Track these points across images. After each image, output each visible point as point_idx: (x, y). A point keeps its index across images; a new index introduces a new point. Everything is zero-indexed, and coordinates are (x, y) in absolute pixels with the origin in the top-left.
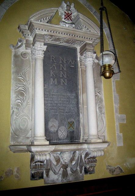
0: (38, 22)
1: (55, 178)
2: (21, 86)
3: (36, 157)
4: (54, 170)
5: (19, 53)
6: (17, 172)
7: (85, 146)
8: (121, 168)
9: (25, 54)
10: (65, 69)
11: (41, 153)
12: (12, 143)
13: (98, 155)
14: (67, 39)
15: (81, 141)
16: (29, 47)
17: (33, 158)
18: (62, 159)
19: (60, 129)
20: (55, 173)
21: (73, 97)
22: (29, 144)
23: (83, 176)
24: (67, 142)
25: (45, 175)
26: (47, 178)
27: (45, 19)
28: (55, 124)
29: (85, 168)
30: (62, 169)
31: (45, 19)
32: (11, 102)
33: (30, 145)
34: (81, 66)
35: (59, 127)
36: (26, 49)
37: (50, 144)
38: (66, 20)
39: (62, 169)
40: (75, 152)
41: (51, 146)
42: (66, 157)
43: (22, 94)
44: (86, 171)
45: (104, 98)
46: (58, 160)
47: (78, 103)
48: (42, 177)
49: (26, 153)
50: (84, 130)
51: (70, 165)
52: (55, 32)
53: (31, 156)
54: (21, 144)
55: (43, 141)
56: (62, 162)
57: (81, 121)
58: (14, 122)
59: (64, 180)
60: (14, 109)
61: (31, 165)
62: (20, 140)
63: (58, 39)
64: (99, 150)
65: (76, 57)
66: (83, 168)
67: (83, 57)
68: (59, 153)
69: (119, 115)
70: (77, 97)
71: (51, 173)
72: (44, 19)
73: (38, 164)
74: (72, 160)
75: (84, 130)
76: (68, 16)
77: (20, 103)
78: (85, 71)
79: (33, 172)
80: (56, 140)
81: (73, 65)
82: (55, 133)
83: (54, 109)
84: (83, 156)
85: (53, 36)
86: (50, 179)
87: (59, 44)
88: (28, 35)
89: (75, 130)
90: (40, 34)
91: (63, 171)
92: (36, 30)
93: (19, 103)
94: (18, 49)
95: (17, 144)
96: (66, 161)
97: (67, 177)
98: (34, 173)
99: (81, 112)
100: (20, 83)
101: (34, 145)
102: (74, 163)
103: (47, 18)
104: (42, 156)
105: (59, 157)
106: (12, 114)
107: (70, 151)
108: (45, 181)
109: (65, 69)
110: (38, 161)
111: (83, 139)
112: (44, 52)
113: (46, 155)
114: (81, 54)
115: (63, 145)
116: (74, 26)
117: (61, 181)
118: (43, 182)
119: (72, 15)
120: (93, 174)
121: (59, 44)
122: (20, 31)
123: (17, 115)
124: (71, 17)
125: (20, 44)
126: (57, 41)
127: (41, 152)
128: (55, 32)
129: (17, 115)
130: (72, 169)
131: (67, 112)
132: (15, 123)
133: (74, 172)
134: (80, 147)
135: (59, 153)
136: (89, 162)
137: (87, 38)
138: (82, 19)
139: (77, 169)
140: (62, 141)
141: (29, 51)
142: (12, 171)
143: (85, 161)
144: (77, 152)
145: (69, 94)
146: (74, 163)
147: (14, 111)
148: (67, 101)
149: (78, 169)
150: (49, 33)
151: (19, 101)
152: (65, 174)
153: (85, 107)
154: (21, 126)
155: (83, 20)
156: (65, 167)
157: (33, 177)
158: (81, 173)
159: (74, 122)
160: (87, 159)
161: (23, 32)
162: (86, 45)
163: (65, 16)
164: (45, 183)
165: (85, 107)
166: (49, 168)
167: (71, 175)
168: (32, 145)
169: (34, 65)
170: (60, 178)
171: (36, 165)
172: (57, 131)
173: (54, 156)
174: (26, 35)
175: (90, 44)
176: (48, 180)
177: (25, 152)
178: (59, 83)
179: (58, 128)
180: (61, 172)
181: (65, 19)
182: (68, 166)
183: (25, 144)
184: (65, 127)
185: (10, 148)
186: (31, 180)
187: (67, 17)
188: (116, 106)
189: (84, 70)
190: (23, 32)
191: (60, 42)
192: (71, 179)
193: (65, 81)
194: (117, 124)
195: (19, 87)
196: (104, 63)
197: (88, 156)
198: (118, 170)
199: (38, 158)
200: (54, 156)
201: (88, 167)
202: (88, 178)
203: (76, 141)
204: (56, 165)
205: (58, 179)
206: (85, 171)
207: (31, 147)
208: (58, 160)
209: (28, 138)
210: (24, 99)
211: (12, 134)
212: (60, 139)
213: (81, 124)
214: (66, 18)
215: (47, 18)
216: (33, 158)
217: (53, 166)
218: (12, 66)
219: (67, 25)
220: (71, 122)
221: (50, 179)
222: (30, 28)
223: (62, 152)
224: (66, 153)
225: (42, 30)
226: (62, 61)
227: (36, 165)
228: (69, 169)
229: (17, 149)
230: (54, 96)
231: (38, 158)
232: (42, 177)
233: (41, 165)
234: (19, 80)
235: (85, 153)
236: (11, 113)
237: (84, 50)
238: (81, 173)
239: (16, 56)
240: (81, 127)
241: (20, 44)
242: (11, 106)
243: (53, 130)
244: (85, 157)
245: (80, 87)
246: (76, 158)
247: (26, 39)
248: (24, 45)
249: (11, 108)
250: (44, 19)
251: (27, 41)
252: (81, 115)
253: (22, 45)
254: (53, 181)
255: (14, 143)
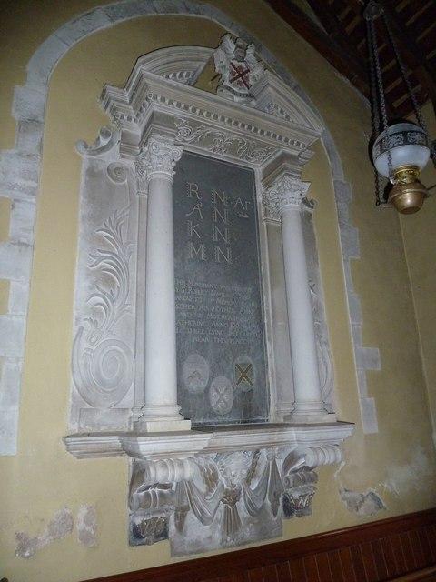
0: (162, 78)
1: (204, 537)
2: (106, 258)
3: (152, 471)
4: (202, 511)
5: (103, 167)
6: (88, 522)
7: (292, 434)
8: (377, 494)
9: (119, 170)
10: (225, 221)
11: (167, 458)
12: (74, 428)
13: (327, 461)
14: (235, 138)
15: (272, 419)
16: (130, 152)
17: (138, 474)
18: (225, 473)
19: (213, 383)
20: (202, 519)
21: (246, 297)
22: (126, 430)
23: (280, 525)
24: (235, 422)
25: (172, 528)
26: (178, 534)
27: (178, 75)
28: (200, 371)
29: (286, 500)
30: (222, 505)
31: (178, 75)
32: (75, 302)
33: (129, 434)
34: (266, 215)
35: (211, 378)
36: (123, 157)
37: (197, 429)
38: (234, 86)
39: (222, 505)
40: (258, 451)
41: (198, 436)
42: (234, 470)
43: (108, 281)
44: (290, 509)
45: (324, 303)
46: (211, 479)
47: (259, 314)
48: (164, 534)
49: (118, 457)
50: (279, 387)
51: (245, 493)
52: (205, 113)
53: (131, 469)
54: (103, 429)
55: (172, 419)
56: (222, 485)
57: (271, 362)
58: (82, 362)
59: (229, 539)
60: (83, 323)
61: (130, 497)
62: (98, 417)
63: (210, 139)
64: (330, 445)
65: (251, 192)
66: (281, 500)
67: (273, 190)
68: (214, 455)
69: (364, 350)
70: (257, 297)
71: (191, 518)
72: (174, 75)
73: (154, 494)
74: (251, 475)
75: (279, 387)
76: (240, 75)
77: (101, 304)
78: (281, 230)
79: (138, 521)
80: (205, 417)
81: (244, 212)
82: (200, 396)
83: (196, 327)
84: (280, 464)
85: (201, 124)
86: (187, 539)
87: (211, 153)
88: (129, 119)
89: (254, 387)
90: (163, 114)
91: (227, 510)
92: (154, 102)
93: (98, 306)
94: (99, 153)
95: (88, 429)
96: (236, 481)
97: (236, 529)
98: (143, 523)
99: (269, 339)
100: (103, 249)
101: (145, 434)
102: (254, 485)
103: (185, 74)
104: (169, 467)
105: (214, 468)
106: (77, 336)
107: (243, 449)
108: (172, 546)
109: (225, 221)
110: (156, 485)
111: (277, 413)
112: (174, 164)
113: (181, 465)
114: (268, 185)
115: (230, 432)
116: (253, 102)
117: (222, 542)
118: (167, 552)
119: (250, 74)
120: (307, 517)
121: (211, 153)
122: (107, 107)
123: (93, 340)
124: (247, 78)
125: (104, 142)
126: (204, 145)
127: (168, 454)
128: (205, 113)
129: (93, 340)
130: (250, 504)
131: (231, 337)
132: (86, 364)
133: (256, 513)
134: (276, 436)
135: (214, 455)
136: (298, 481)
137: (286, 141)
138: (273, 88)
139: (264, 505)
140: (220, 419)
141: (130, 163)
142: (71, 518)
143: (287, 478)
144: (264, 452)
145: (238, 289)
146: (254, 485)
147: (81, 328)
148: (233, 307)
149: (268, 502)
150: (189, 115)
151: (101, 300)
152: (231, 522)
153: (279, 323)
154: (104, 375)
155: (278, 91)
156: (231, 497)
157: (137, 534)
158: (275, 514)
159: (250, 365)
160: (292, 472)
161: (114, 110)
162: (284, 157)
163: (232, 73)
164: (174, 553)
165: (279, 323)
166: (185, 504)
167: (248, 523)
168: (138, 432)
169: (144, 203)
170: (217, 536)
171: (147, 495)
172: (207, 390)
173: (200, 467)
174: (122, 117)
175: (292, 157)
176: (183, 543)
177: (115, 455)
178: (210, 255)
179: (210, 382)
180: (219, 515)
181: (231, 81)
182: (240, 493)
183: (113, 429)
184: (229, 378)
185: (66, 443)
186: (130, 544)
187: (237, 78)
188: (354, 325)
189: (272, 226)
190: (114, 110)
191: (214, 150)
192: (249, 537)
193: (225, 253)
194: (358, 373)
195: (101, 259)
196: (393, 162)
197: (296, 462)
198: (369, 502)
199: (157, 474)
200: (200, 467)
201: (296, 495)
202: (294, 529)
203: (258, 421)
204: (207, 494)
205: (210, 538)
206: (285, 506)
207: (139, 439)
208: (211, 479)
209: (124, 410)
210: (115, 294)
211: (74, 398)
212: (215, 415)
213: (270, 372)
214: (235, 79)
215: (185, 74)
216: (138, 474)
217: (198, 498)
218: (82, 198)
219: (237, 99)
220: (243, 365)
221: (187, 539)
222: (136, 96)
223: (222, 452)
224: (236, 456)
225: (171, 103)
226: (218, 199)
227: (147, 495)
228: (241, 504)
229: (89, 447)
230: (197, 292)
231: (157, 474)
232: (164, 534)
233: (162, 495)
234: (101, 240)
235: (285, 455)
236: (74, 334)
237: (271, 174)
238: (275, 514)
239: (92, 173)
240: (270, 379)
241: (104, 142)
242: (75, 313)
243: (194, 387)
244: (286, 467)
245: (265, 269)
246: (261, 470)
247: (124, 130)
248: (116, 147)
249: (74, 320)
250: (174, 75)
251: (124, 135)
252: (269, 347)
253: (111, 143)
254: (197, 543)
255: (80, 428)
